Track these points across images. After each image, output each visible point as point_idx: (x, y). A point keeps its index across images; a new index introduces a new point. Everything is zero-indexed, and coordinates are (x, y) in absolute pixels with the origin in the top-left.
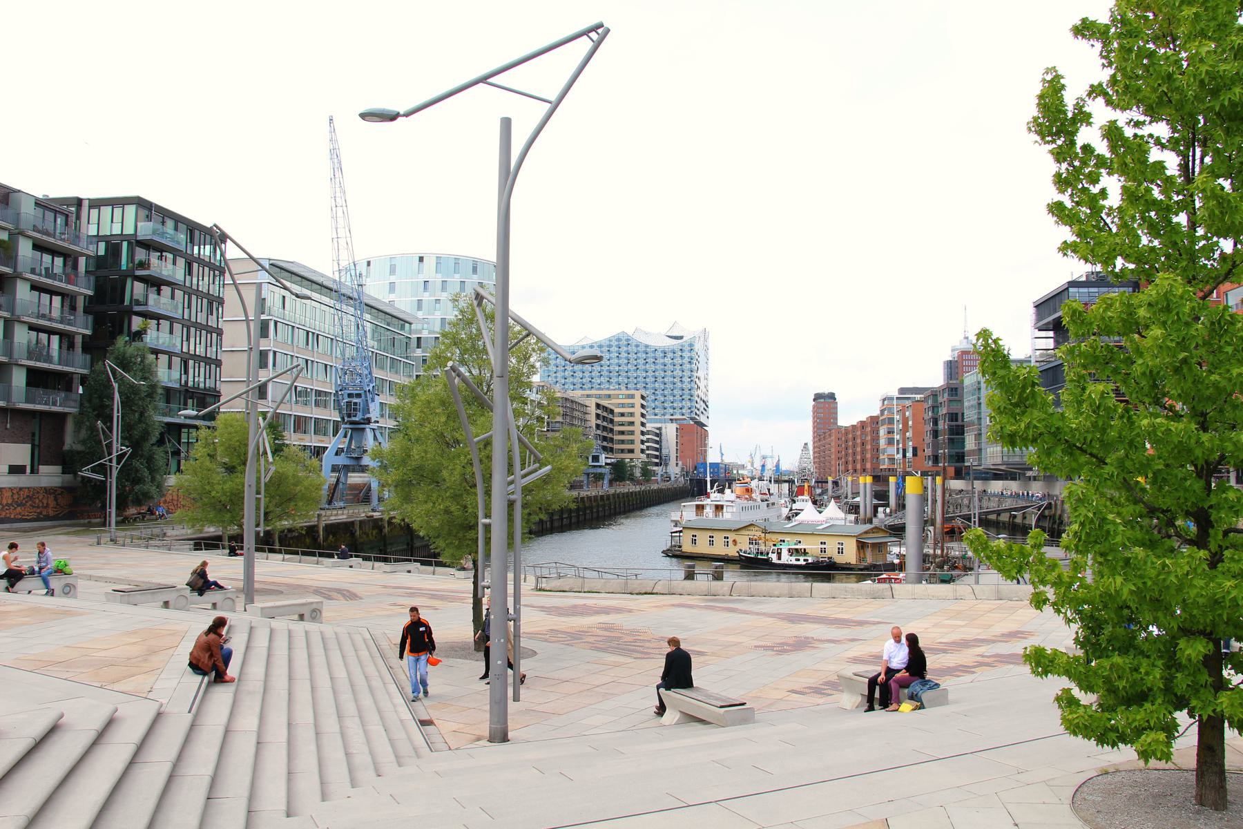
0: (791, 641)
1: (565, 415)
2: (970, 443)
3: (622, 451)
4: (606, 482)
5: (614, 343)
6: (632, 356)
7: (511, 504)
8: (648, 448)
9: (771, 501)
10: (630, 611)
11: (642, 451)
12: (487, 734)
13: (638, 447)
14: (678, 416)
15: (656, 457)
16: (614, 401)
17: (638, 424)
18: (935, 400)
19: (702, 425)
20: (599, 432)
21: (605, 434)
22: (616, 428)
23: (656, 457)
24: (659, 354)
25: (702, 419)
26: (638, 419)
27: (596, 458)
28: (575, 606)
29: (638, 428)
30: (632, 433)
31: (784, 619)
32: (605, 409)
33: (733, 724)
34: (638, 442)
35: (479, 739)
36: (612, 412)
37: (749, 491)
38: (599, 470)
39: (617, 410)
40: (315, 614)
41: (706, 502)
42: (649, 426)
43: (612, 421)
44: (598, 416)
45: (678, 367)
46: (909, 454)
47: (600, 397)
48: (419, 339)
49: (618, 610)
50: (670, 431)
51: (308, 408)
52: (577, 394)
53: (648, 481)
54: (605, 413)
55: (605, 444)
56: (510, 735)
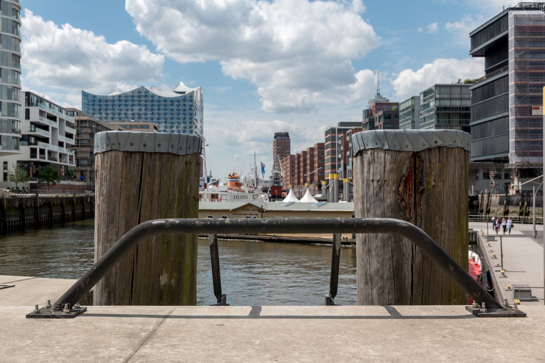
45: (182, 112)
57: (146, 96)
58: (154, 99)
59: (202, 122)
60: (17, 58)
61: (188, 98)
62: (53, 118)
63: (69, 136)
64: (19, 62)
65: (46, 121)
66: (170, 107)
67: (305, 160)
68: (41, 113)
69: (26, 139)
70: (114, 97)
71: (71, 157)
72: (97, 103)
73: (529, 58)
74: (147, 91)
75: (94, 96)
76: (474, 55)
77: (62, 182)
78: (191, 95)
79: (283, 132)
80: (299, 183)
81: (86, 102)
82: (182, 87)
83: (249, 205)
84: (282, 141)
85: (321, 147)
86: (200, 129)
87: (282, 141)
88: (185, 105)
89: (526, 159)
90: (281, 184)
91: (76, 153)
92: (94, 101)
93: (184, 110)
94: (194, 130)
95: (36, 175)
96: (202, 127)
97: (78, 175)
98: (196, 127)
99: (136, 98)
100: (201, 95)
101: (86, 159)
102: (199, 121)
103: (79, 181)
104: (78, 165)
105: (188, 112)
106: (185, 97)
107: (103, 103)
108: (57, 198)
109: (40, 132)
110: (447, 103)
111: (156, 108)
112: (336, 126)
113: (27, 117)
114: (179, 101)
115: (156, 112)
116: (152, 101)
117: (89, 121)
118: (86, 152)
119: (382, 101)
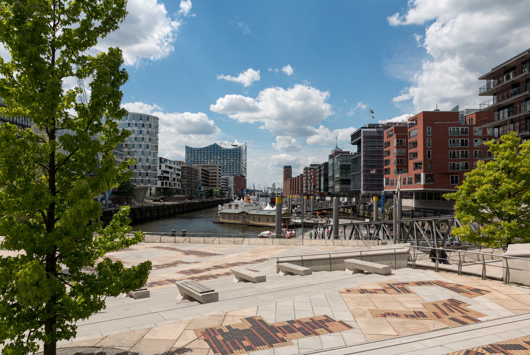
1: (188, 173)
2: (331, 184)
3: (212, 186)
5: (212, 147)
6: (219, 152)
11: (220, 186)
13: (218, 184)
17: (218, 176)
18: (320, 169)
22: (210, 178)
23: (227, 188)
24: (228, 151)
25: (244, 175)
26: (218, 175)
27: (200, 189)
29: (218, 178)
30: (216, 179)
32: (205, 171)
36: (208, 172)
37: (249, 199)
41: (233, 203)
42: (223, 177)
43: (208, 175)
46: (312, 188)
47: (204, 166)
48: (126, 144)
50: (231, 179)
52: (195, 166)
53: (222, 197)
54: (206, 173)
59: (246, 160)
61: (238, 149)
62: (171, 168)
63: (178, 175)
65: (168, 170)
67: (298, 180)
68: (166, 166)
69: (160, 177)
71: (179, 185)
72: (193, 151)
73: (370, 149)
75: (192, 148)
76: (353, 144)
77: (175, 196)
78: (240, 147)
80: (293, 193)
82: (236, 143)
84: (288, 170)
85: (302, 175)
87: (288, 170)
89: (368, 192)
91: (182, 173)
95: (163, 194)
96: (246, 163)
97: (182, 192)
99: (212, 149)
100: (246, 147)
104: (182, 187)
105: (238, 156)
109: (165, 175)
110: (345, 163)
111: (222, 154)
112: (309, 166)
113: (160, 168)
115: (222, 156)
119: (338, 150)
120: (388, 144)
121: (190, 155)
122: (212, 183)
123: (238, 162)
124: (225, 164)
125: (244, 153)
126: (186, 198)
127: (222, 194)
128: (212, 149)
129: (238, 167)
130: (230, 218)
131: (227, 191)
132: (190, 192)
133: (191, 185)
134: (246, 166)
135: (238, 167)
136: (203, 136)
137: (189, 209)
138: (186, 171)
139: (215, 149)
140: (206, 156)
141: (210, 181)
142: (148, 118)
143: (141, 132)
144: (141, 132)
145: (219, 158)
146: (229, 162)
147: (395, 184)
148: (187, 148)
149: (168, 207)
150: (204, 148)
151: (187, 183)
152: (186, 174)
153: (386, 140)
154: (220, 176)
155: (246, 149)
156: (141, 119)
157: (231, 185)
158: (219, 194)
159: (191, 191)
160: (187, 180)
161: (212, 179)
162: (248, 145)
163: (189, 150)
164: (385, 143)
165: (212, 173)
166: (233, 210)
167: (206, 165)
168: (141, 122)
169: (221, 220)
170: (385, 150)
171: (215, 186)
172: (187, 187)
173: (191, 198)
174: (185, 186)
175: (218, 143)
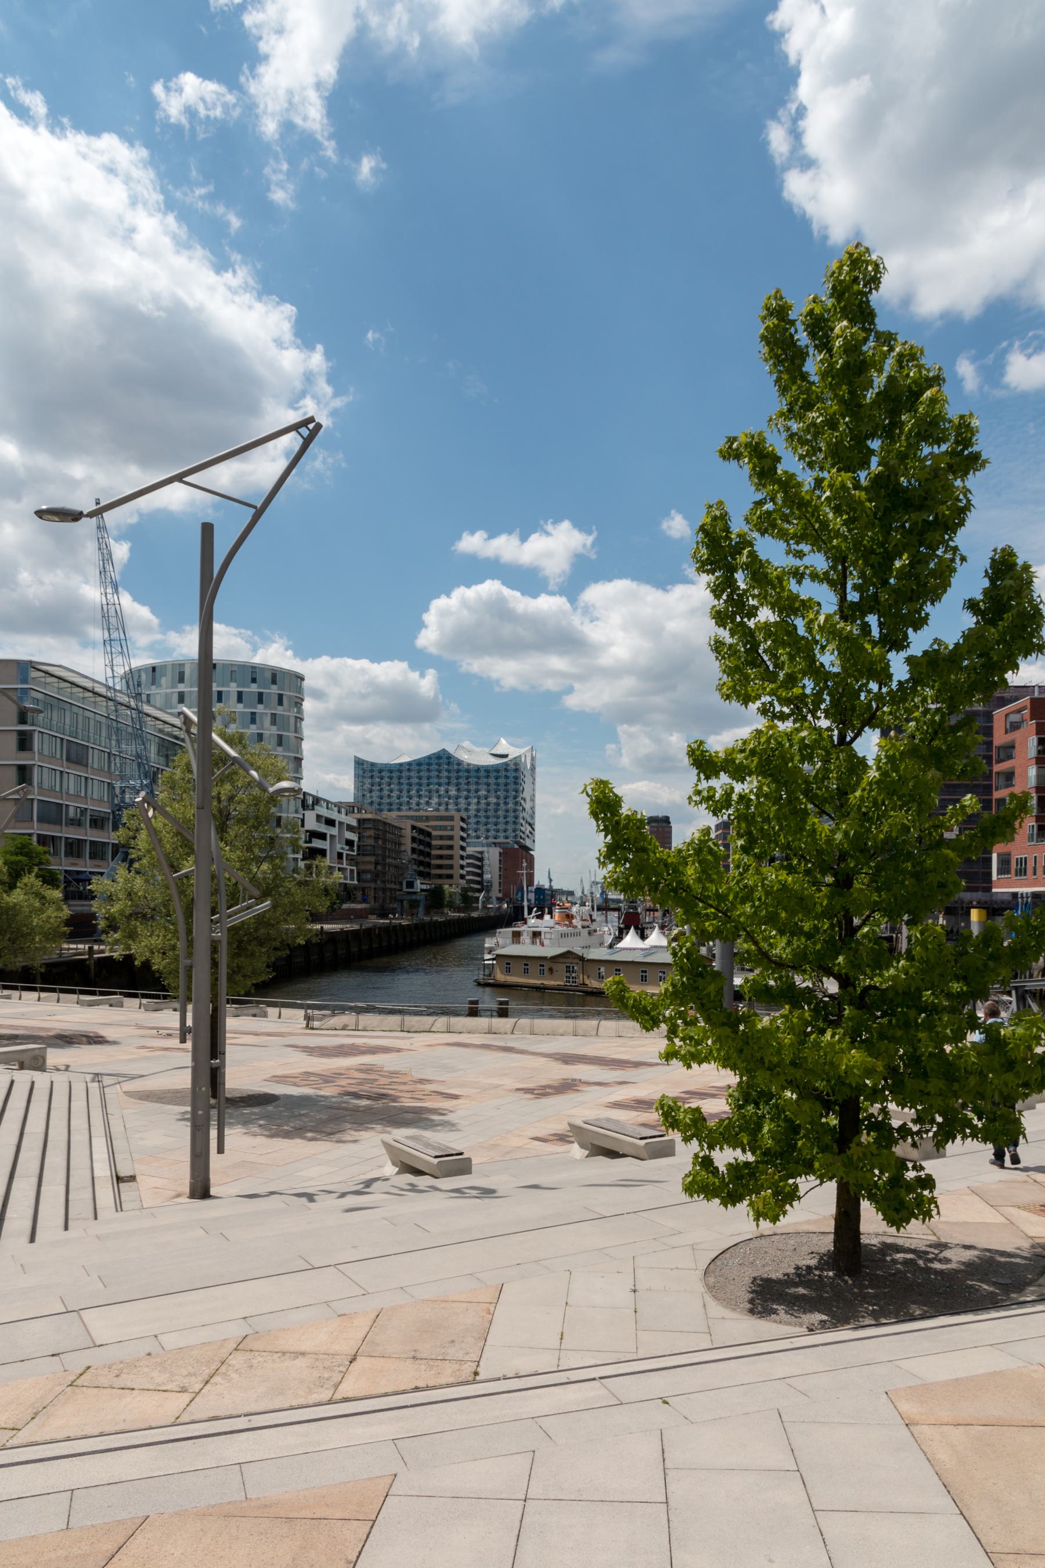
0: (556, 1084)
1: (376, 838)
3: (440, 876)
4: (421, 909)
7: (214, 948)
8: (468, 873)
9: (593, 927)
10: (399, 1050)
11: (462, 877)
12: (187, 1190)
13: (457, 872)
14: (501, 840)
15: (478, 883)
16: (432, 823)
17: (457, 847)
19: (527, 849)
20: (415, 856)
21: (421, 858)
22: (434, 852)
23: (478, 883)
24: (482, 773)
25: (528, 843)
26: (457, 843)
27: (411, 885)
28: (342, 1046)
29: (457, 852)
30: (451, 857)
31: (557, 1059)
32: (421, 831)
33: (456, 1175)
34: (456, 867)
35: (178, 1196)
36: (429, 834)
37: (569, 917)
38: (414, 897)
39: (434, 833)
40: (38, 1063)
41: (523, 928)
42: (470, 850)
43: (429, 845)
44: (414, 839)
45: (502, 787)
47: (419, 819)
49: (386, 1050)
50: (492, 856)
51: (81, 830)
52: (391, 817)
54: (422, 837)
55: (421, 868)
56: (213, 1191)
57: (449, 764)
58: (461, 767)
59: (533, 800)
60: (298, 760)
63: (350, 843)
64: (301, 766)
65: (322, 828)
66: (485, 780)
70: (401, 765)
71: (352, 871)
74: (449, 757)
75: (373, 764)
79: (660, 815)
81: (361, 772)
82: (504, 746)
83: (569, 952)
86: (530, 812)
88: (507, 777)
90: (639, 910)
92: (372, 771)
93: (506, 785)
94: (521, 815)
96: (533, 808)
97: (359, 894)
98: (524, 809)
99: (434, 767)
100: (533, 759)
101: (369, 871)
102: (528, 799)
103: (360, 903)
104: (359, 880)
105: (512, 787)
106: (506, 764)
107: (385, 774)
108: (342, 931)
109: (317, 844)
111: (463, 781)
114: (498, 771)
116: (458, 771)
117: (374, 820)
118: (369, 862)
120: (1008, 751)
121: (367, 786)
122: (440, 867)
123: (511, 806)
124: (472, 813)
125: (528, 779)
126: (372, 911)
127: (467, 900)
128: (434, 767)
129: (510, 819)
130: (526, 971)
131: (480, 891)
132: (380, 894)
133: (384, 873)
134: (532, 817)
135: (510, 819)
136: (408, 729)
137: (385, 944)
138: (371, 833)
139: (441, 764)
140: (415, 788)
141: (434, 862)
142: (275, 676)
143: (253, 718)
144: (253, 718)
145: (453, 792)
146: (483, 806)
147: (1030, 871)
148: (359, 763)
149: (332, 937)
150: (409, 764)
151: (372, 867)
152: (371, 842)
153: (1000, 738)
154: (463, 848)
155: (533, 768)
156: (254, 680)
157: (492, 873)
158: (458, 901)
159: (384, 890)
160: (373, 859)
161: (441, 857)
162: (539, 756)
163: (365, 770)
164: (999, 748)
165: (441, 838)
166: (526, 948)
167: (422, 813)
168: (254, 688)
169: (500, 977)
170: (997, 768)
171: (450, 877)
172: (375, 881)
173: (384, 915)
174: (369, 876)
175: (451, 749)
